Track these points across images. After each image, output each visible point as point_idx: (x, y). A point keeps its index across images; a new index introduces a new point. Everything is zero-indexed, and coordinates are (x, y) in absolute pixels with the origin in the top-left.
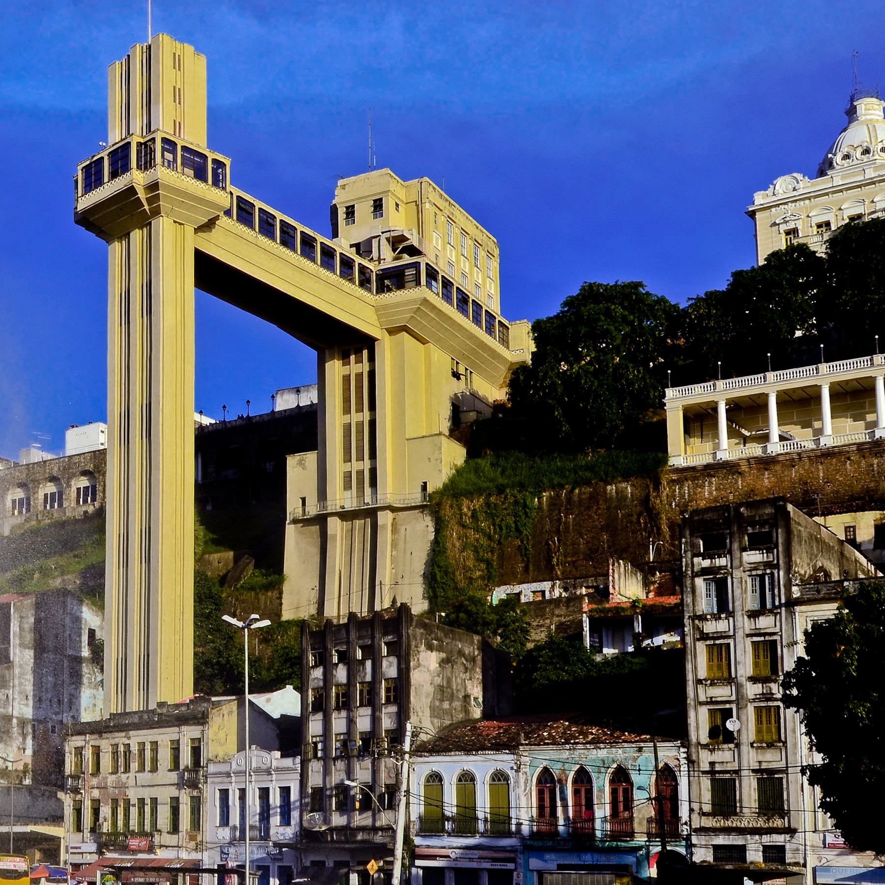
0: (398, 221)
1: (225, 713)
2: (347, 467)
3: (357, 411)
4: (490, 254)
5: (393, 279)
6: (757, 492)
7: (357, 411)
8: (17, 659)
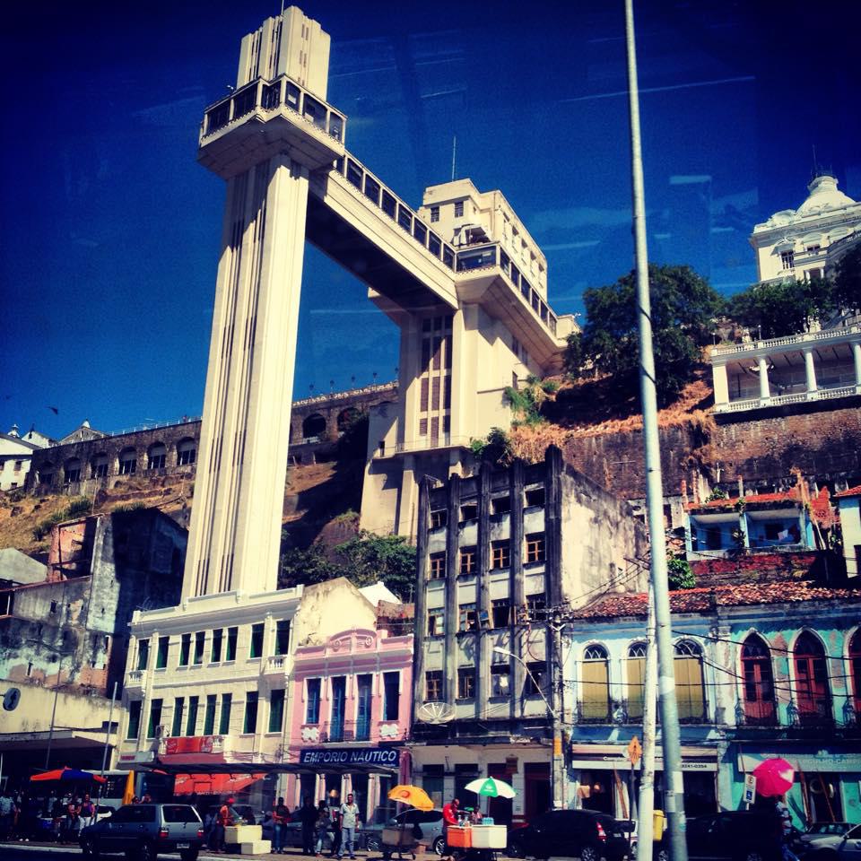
0: (473, 219)
1: (320, 592)
2: (424, 415)
3: (434, 369)
4: (541, 269)
5: (468, 262)
6: (799, 433)
7: (434, 369)
8: (97, 572)
